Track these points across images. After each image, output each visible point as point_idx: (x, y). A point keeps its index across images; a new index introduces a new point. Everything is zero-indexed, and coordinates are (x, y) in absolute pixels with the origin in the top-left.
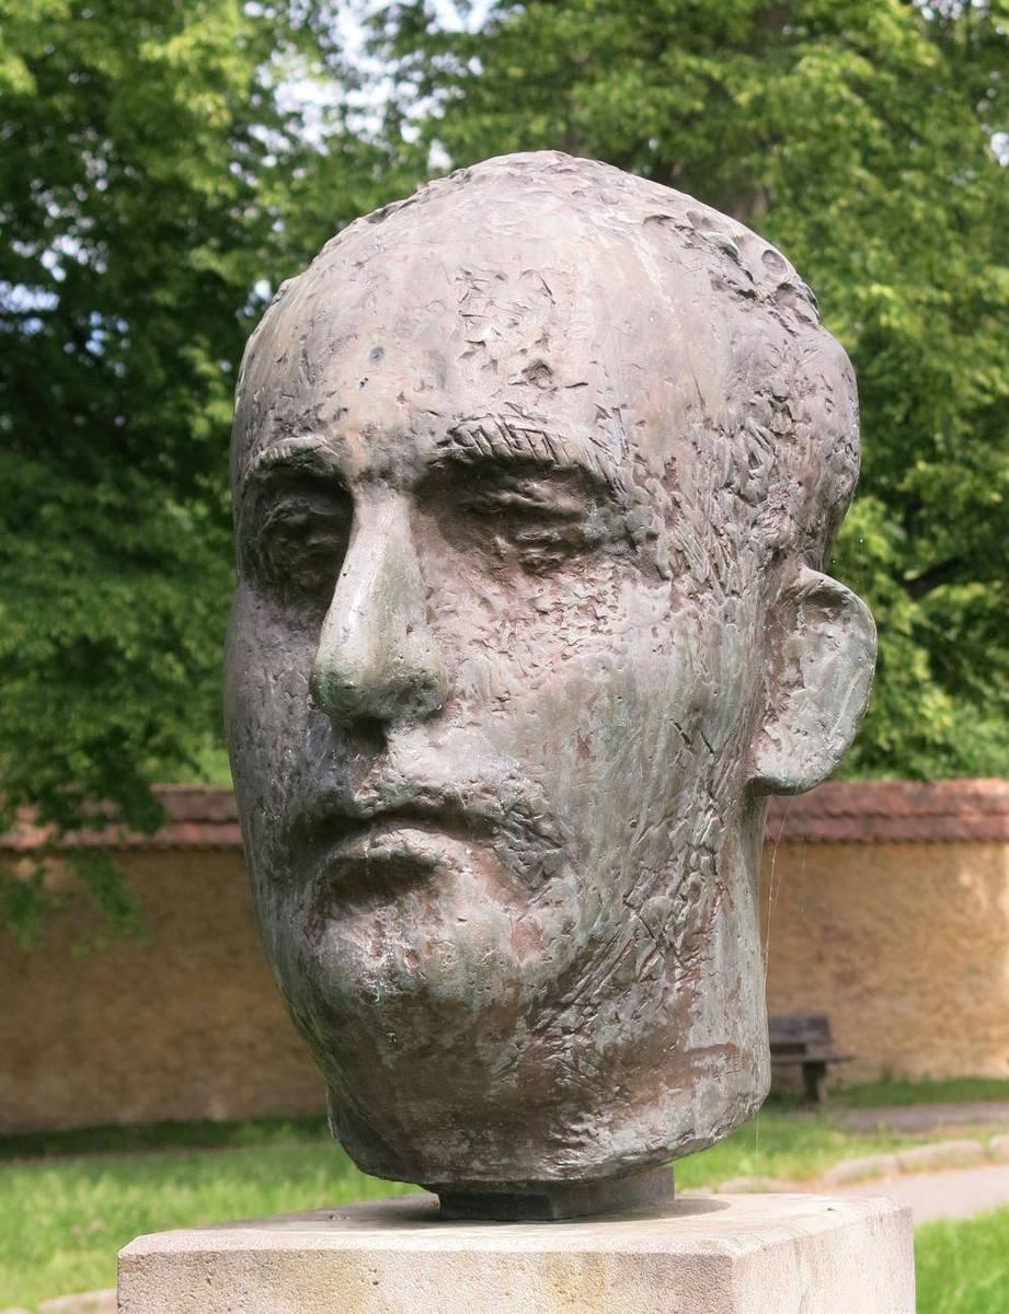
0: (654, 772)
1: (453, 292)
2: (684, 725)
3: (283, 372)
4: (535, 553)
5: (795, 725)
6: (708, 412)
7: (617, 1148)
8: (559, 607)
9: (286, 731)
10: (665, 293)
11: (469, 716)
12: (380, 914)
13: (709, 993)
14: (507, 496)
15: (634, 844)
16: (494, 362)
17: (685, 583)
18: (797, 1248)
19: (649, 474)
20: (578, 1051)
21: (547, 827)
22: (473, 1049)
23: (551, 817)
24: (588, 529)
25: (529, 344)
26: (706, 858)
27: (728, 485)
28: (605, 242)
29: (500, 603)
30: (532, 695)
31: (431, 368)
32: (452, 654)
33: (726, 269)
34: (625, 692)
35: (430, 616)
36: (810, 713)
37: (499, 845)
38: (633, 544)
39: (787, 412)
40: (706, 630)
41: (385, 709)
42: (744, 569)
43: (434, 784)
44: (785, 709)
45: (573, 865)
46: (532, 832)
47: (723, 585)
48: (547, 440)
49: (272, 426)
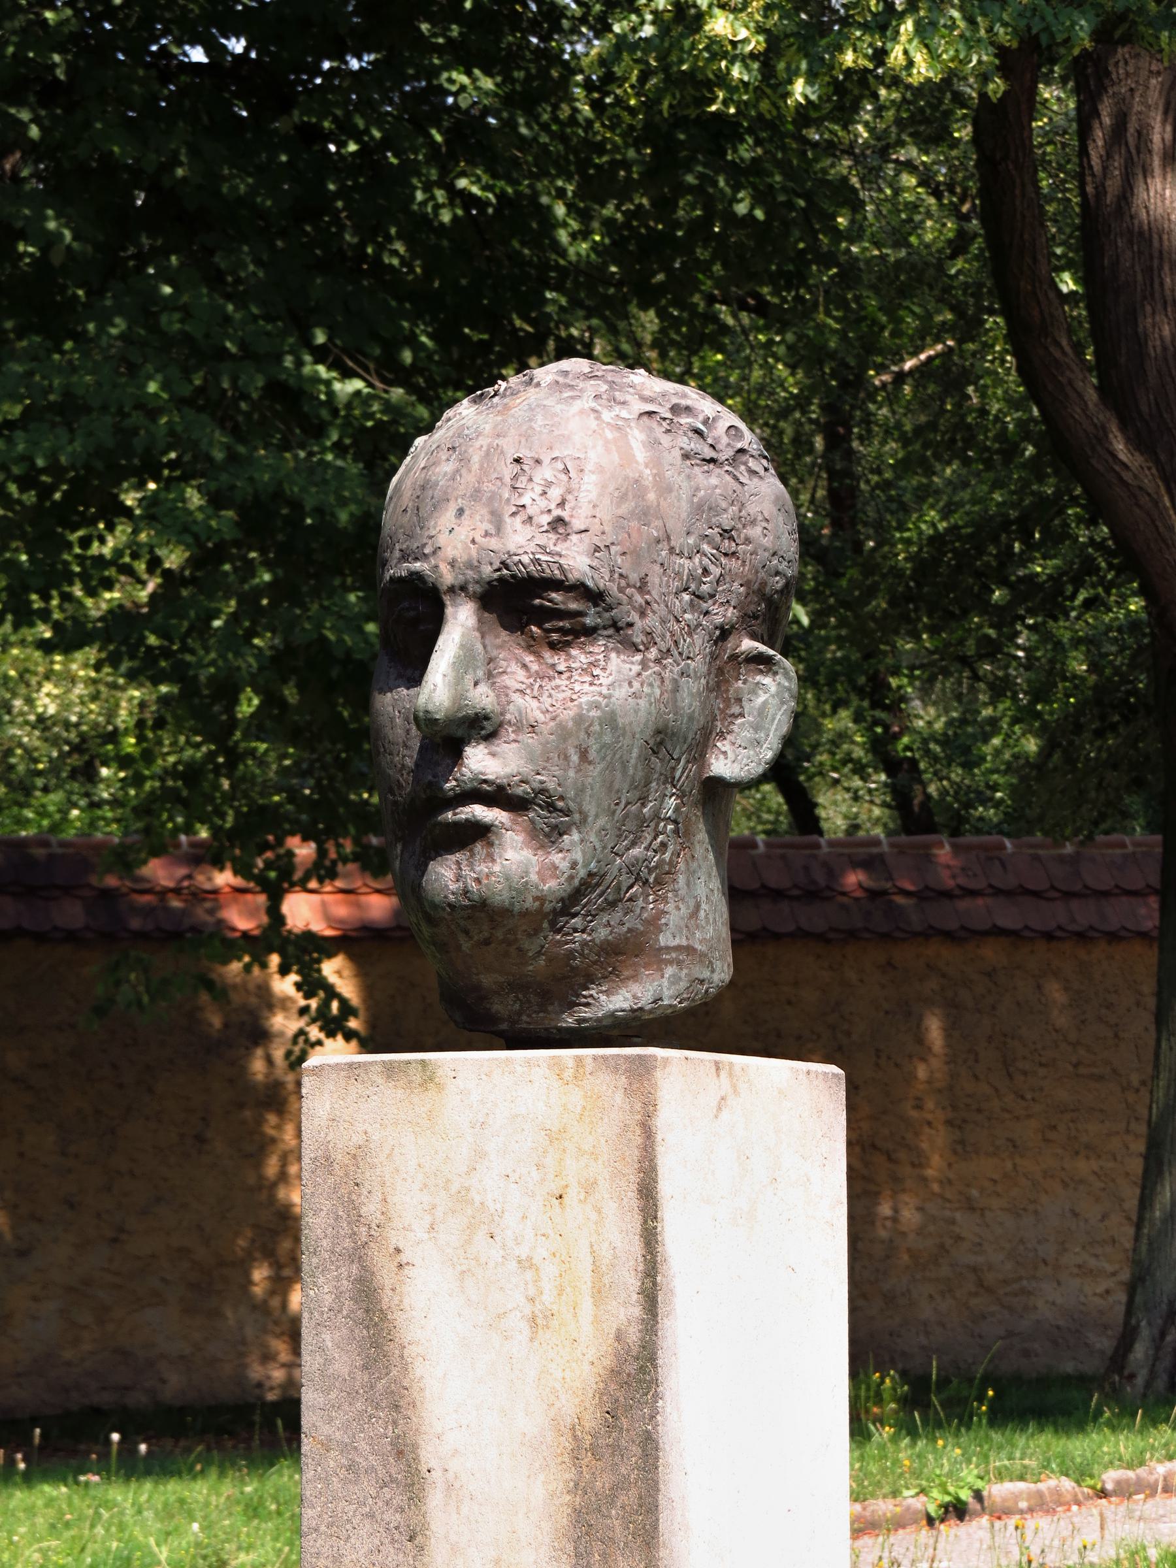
0: (631, 772)
1: (509, 470)
2: (651, 742)
3: (405, 519)
4: (555, 636)
5: (739, 742)
6: (673, 543)
7: (612, 1007)
8: (570, 669)
9: (406, 746)
10: (647, 466)
11: (512, 736)
12: (458, 856)
13: (675, 914)
14: (537, 601)
15: (619, 814)
16: (530, 518)
17: (653, 653)
18: (718, 1069)
19: (628, 586)
20: (584, 944)
21: (560, 804)
22: (516, 940)
23: (562, 798)
24: (588, 621)
25: (553, 506)
26: (670, 827)
27: (686, 590)
28: (609, 435)
29: (534, 667)
30: (552, 724)
31: (491, 522)
32: (503, 699)
33: (695, 445)
34: (610, 720)
35: (490, 675)
36: (747, 734)
37: (531, 815)
38: (618, 629)
39: (732, 538)
40: (667, 682)
41: (460, 733)
42: (699, 643)
43: (491, 777)
44: (729, 732)
45: (578, 828)
46: (550, 807)
47: (680, 654)
48: (561, 567)
49: (397, 554)
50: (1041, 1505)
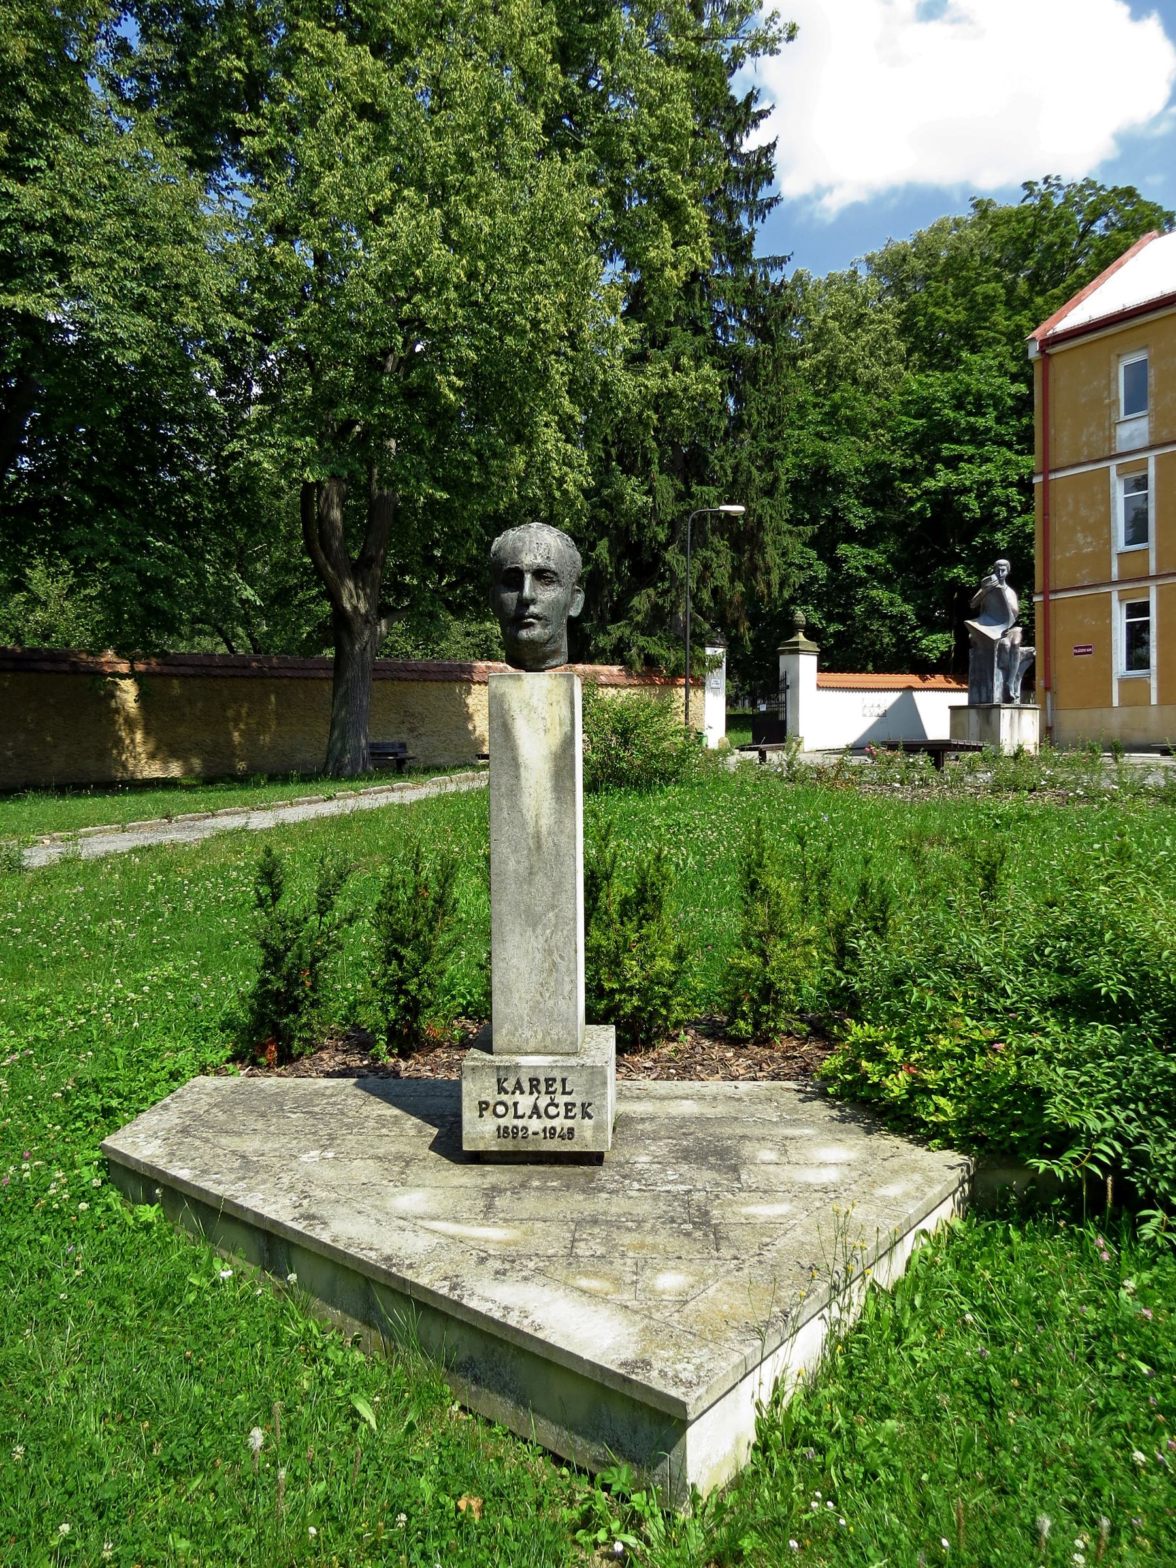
50: (349, 797)
